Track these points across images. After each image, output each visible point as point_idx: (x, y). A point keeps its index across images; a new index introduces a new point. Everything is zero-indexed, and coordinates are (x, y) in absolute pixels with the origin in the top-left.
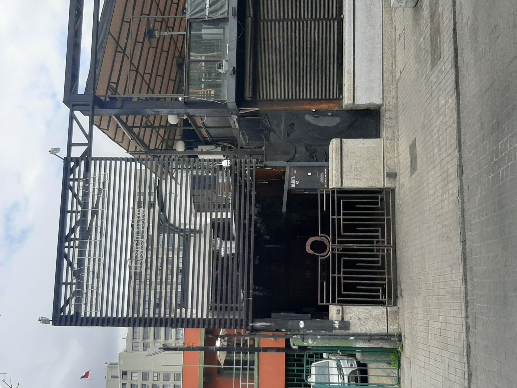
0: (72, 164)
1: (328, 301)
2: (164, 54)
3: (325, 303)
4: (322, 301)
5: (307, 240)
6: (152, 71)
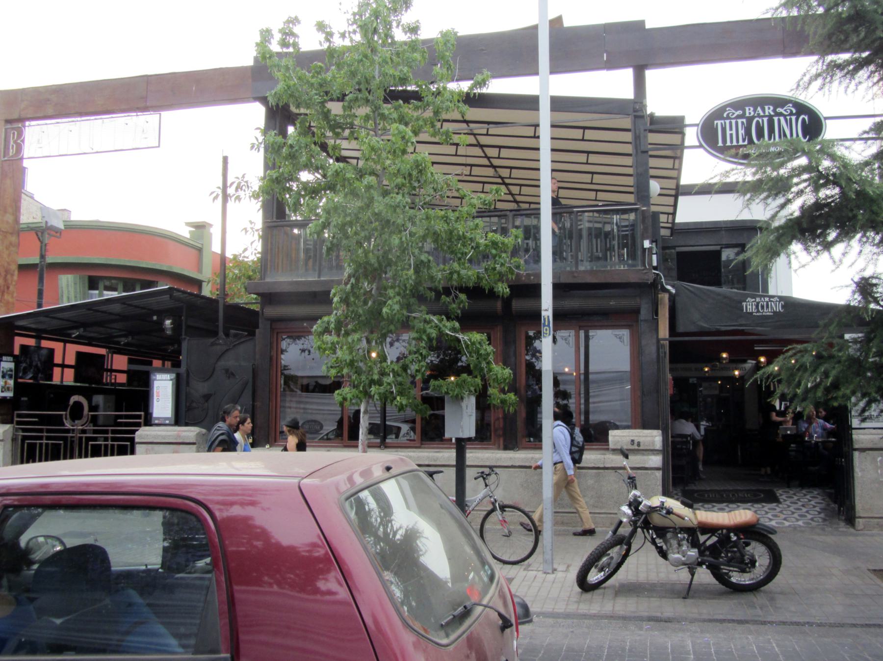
0: (826, 163)
1: (19, 423)
2: (593, 158)
3: (16, 419)
4: (19, 416)
5: (84, 396)
6: (466, 165)
